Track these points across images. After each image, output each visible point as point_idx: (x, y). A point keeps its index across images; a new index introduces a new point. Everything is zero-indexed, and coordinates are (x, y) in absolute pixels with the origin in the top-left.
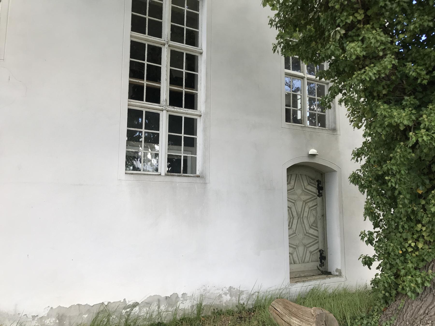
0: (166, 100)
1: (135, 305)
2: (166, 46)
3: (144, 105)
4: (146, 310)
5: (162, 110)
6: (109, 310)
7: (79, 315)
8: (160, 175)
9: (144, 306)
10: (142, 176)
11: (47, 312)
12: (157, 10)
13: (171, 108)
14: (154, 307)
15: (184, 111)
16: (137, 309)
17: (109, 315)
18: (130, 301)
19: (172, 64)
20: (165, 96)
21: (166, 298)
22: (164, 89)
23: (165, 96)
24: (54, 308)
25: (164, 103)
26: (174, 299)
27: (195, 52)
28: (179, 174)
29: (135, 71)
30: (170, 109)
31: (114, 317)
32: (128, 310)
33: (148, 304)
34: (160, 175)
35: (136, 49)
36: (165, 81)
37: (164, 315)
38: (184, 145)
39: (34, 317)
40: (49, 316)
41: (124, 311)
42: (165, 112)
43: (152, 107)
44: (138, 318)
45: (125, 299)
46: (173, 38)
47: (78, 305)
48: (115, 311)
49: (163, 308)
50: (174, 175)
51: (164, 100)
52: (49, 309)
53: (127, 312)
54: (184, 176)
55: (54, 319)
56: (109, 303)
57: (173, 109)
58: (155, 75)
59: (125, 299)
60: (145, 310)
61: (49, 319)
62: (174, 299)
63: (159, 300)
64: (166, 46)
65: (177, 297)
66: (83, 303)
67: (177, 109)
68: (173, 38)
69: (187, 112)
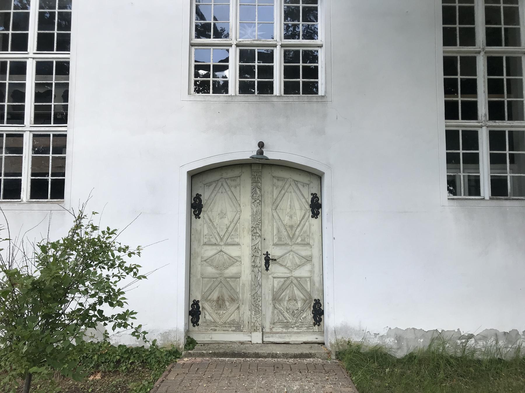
0: (485, 115)
1: (471, 336)
2: (482, 53)
3: (461, 124)
4: (483, 343)
5: (481, 127)
6: (443, 338)
7: (415, 338)
8: (484, 199)
9: (480, 339)
10: (466, 201)
11: (386, 331)
12: (468, 15)
13: (491, 123)
14: (491, 342)
15: (509, 124)
16: (472, 342)
17: (444, 343)
18: (465, 331)
19: (490, 72)
20: (483, 109)
21: (505, 333)
22: (322, 79)
23: (483, 109)
24: (392, 328)
25: (483, 119)
26: (514, 336)
27: (518, 52)
28: (506, 197)
29: (450, 87)
30: (491, 124)
31: (448, 345)
32: (464, 341)
33: (484, 337)
34: (484, 199)
35: (449, 65)
36: (483, 94)
37: (505, 351)
38: (463, 163)
39: (376, 335)
40: (388, 336)
41: (459, 342)
42: (484, 128)
43: (470, 124)
44: (474, 351)
45: (458, 329)
46: (489, 43)
47: (413, 329)
48: (450, 339)
49: (501, 343)
50: (500, 199)
51: (483, 115)
52: (388, 329)
53: (462, 343)
54: (513, 199)
55: (393, 339)
56: (443, 331)
57: (494, 124)
58: (470, 87)
59: (458, 329)
60: (481, 343)
61: (389, 339)
62: (514, 336)
63: (496, 335)
64: (482, 53)
65: (518, 334)
66: (418, 328)
67: (498, 123)
68: (489, 43)
69: (512, 124)
